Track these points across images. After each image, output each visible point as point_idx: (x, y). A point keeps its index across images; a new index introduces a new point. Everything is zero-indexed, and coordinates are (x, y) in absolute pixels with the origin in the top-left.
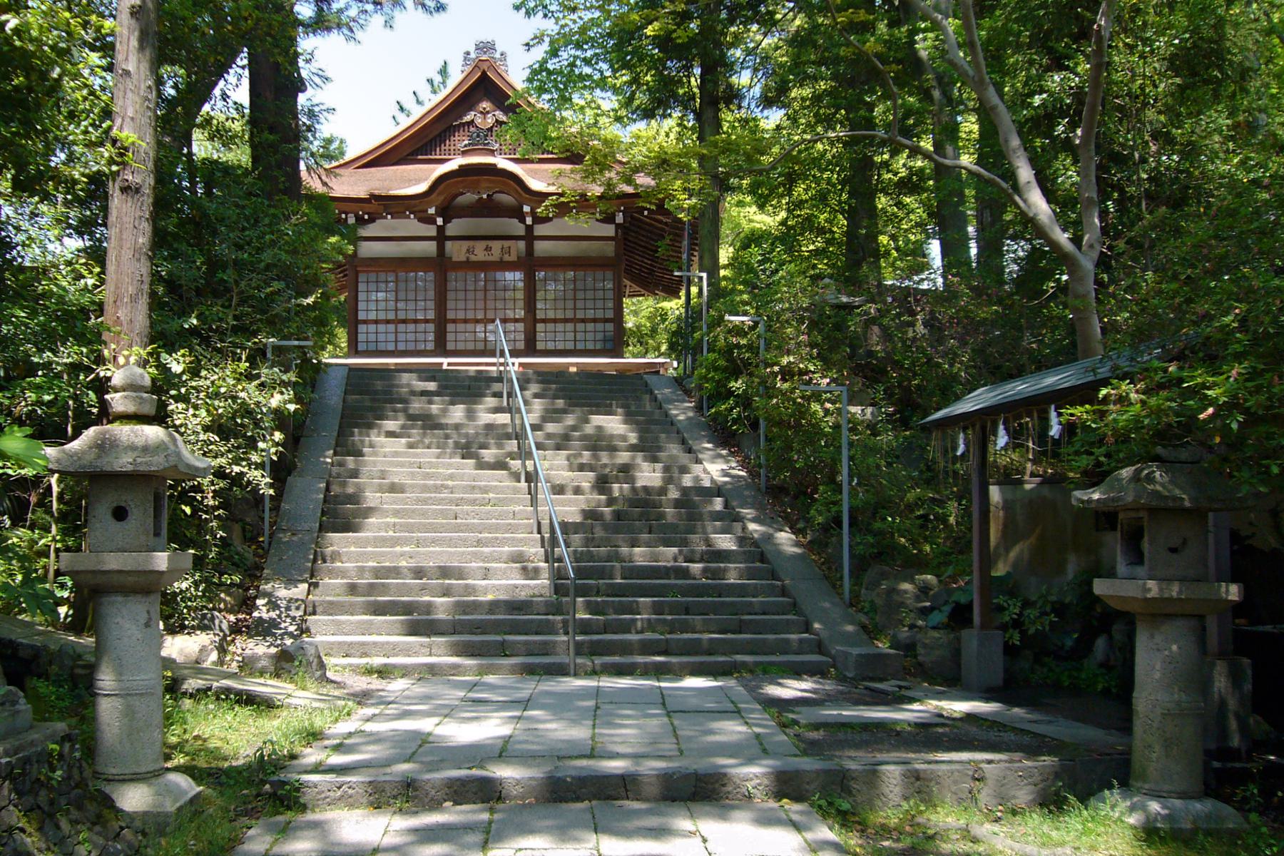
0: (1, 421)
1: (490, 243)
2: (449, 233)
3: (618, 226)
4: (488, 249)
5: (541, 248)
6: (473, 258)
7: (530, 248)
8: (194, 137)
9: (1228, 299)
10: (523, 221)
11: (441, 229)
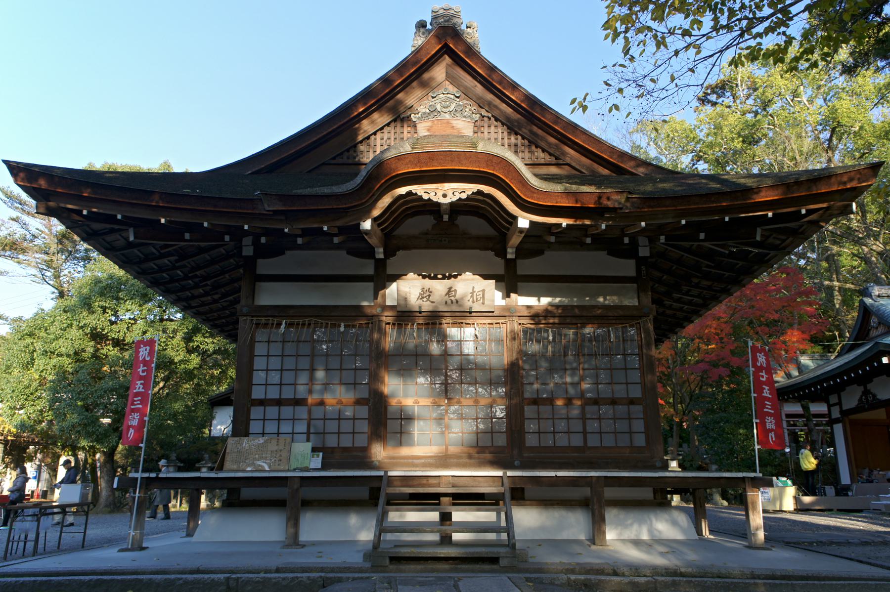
3: (641, 262)
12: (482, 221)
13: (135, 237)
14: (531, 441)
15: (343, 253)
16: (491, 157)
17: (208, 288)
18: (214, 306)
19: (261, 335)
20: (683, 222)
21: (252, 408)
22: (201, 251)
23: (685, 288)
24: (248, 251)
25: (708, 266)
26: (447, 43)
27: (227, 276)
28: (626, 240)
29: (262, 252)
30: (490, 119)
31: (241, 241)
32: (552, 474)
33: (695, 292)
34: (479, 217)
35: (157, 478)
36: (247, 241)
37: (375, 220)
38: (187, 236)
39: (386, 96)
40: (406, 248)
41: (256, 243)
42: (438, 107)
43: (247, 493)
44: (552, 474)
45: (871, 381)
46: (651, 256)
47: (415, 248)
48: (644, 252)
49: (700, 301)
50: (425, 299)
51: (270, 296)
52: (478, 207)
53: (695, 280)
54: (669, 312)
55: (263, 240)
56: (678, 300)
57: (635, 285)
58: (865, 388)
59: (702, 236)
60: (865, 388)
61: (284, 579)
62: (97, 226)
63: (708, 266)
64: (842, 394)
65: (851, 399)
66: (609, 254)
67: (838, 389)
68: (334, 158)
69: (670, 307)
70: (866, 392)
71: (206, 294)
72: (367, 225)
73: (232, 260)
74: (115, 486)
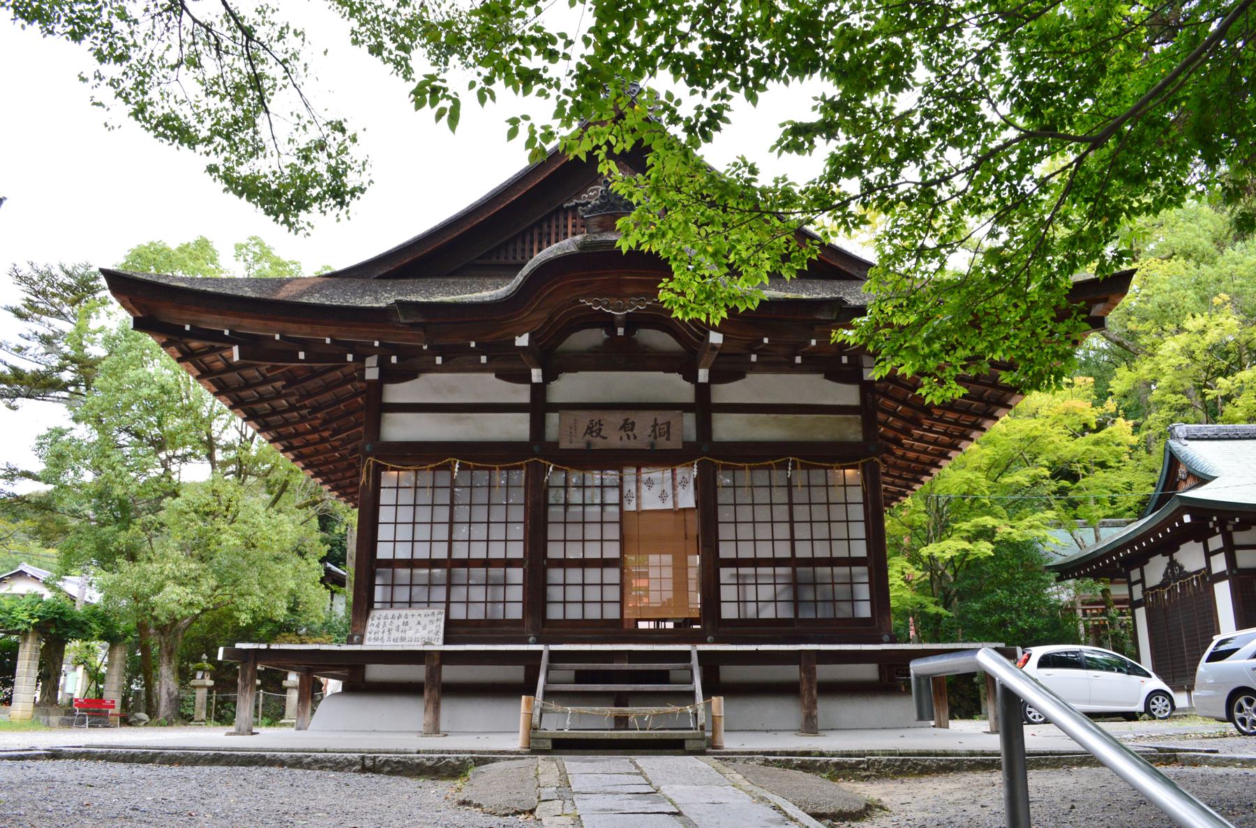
1: (633, 416)
5: (727, 428)
6: (599, 443)
7: (704, 427)
10: (691, 376)
11: (538, 391)
13: (240, 357)
14: (729, 612)
15: (491, 376)
17: (317, 422)
18: (320, 447)
27: (342, 406)
28: (845, 360)
29: (390, 375)
31: (364, 362)
32: (753, 648)
34: (663, 331)
35: (268, 650)
36: (372, 361)
41: (383, 365)
43: (376, 672)
44: (753, 648)
45: (1177, 549)
51: (399, 428)
54: (911, 455)
55: (394, 359)
56: (921, 439)
58: (1171, 558)
60: (1171, 558)
61: (428, 759)
64: (1145, 567)
65: (1156, 571)
67: (1140, 560)
68: (480, 258)
69: (911, 448)
70: (1173, 564)
71: (314, 430)
74: (238, 646)
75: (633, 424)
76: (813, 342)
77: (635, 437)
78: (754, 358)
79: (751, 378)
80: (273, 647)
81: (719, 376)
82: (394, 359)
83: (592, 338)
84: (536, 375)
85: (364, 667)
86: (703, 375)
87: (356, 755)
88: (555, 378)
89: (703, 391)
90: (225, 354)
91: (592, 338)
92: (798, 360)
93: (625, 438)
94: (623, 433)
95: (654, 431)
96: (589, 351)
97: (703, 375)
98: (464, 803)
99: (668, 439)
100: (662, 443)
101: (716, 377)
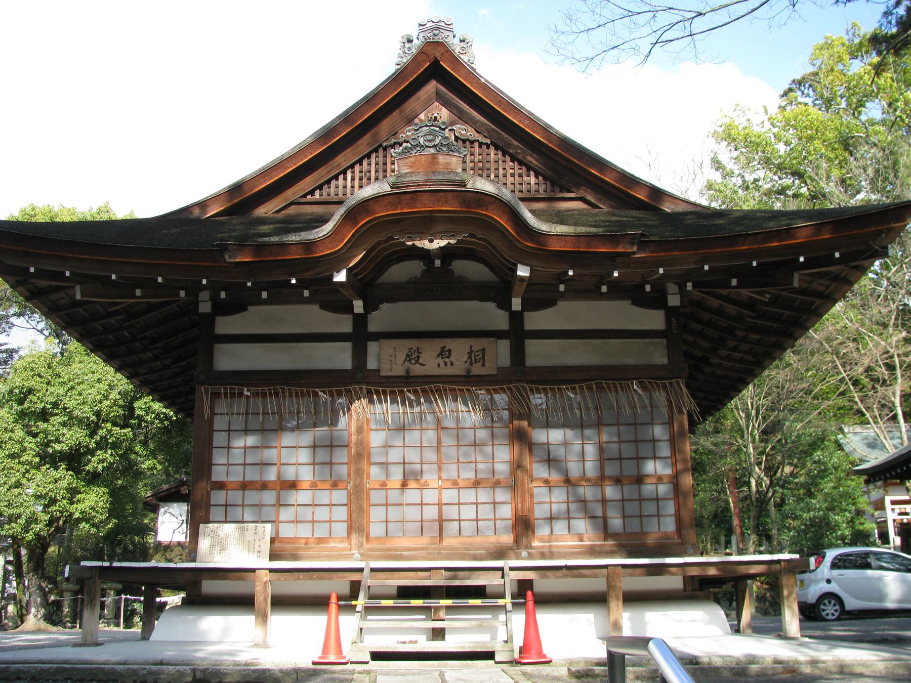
0: (910, 154)
1: (449, 343)
2: (372, 328)
3: (671, 313)
4: (444, 353)
5: (539, 353)
6: (417, 370)
7: (518, 353)
8: (109, 373)
9: (737, 431)
10: (505, 305)
11: (360, 321)
12: (481, 267)
16: (483, 196)
19: (222, 406)
20: (706, 268)
21: (213, 492)
22: (151, 308)
23: (731, 343)
24: (205, 307)
25: (750, 317)
26: (433, 70)
28: (648, 288)
29: (222, 309)
30: (488, 147)
31: (197, 296)
33: (744, 347)
34: (478, 262)
35: (111, 568)
36: (204, 296)
37: (350, 271)
38: (138, 292)
39: (362, 129)
40: (392, 299)
41: (214, 299)
42: (422, 140)
46: (682, 306)
47: (401, 300)
48: (674, 300)
49: (749, 358)
50: (413, 362)
51: (229, 358)
52: (472, 250)
53: (740, 334)
55: (223, 295)
56: (728, 358)
57: (665, 341)
59: (734, 282)
62: (42, 283)
63: (750, 317)
66: (634, 303)
68: (305, 196)
72: (341, 277)
73: (186, 318)
74: (83, 563)
75: (450, 351)
76: (616, 274)
77: (452, 364)
78: (562, 288)
79: (563, 305)
80: (116, 564)
81: (531, 304)
82: (223, 295)
83: (410, 269)
84: (358, 306)
85: (200, 582)
86: (516, 304)
87: (187, 668)
88: (376, 308)
89: (516, 318)
90: (70, 292)
91: (410, 269)
92: (604, 289)
93: (442, 364)
94: (440, 360)
95: (470, 357)
96: (408, 282)
97: (516, 304)
98: (692, 621)
99: (483, 365)
100: (477, 370)
101: (528, 305)
